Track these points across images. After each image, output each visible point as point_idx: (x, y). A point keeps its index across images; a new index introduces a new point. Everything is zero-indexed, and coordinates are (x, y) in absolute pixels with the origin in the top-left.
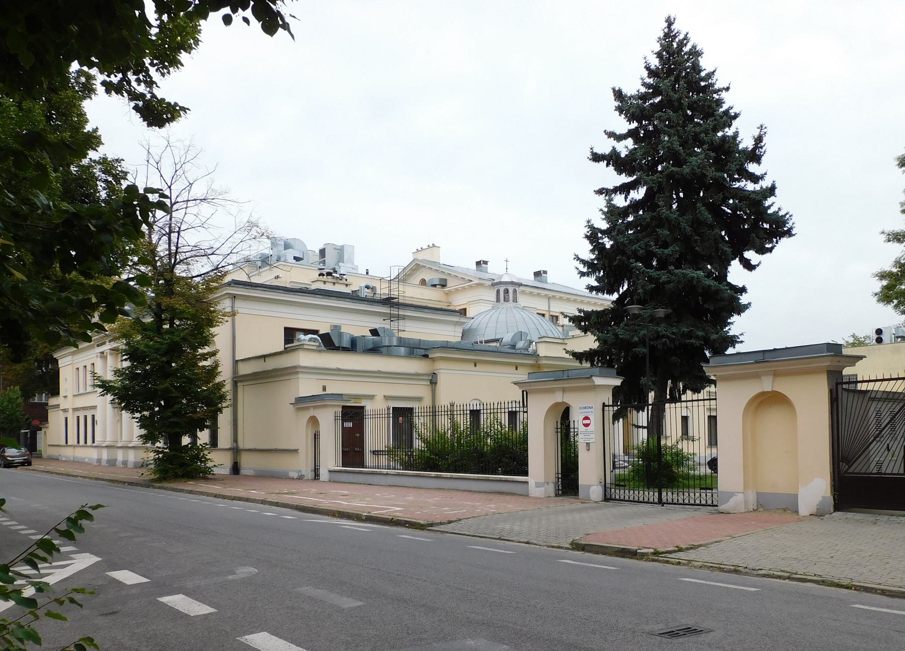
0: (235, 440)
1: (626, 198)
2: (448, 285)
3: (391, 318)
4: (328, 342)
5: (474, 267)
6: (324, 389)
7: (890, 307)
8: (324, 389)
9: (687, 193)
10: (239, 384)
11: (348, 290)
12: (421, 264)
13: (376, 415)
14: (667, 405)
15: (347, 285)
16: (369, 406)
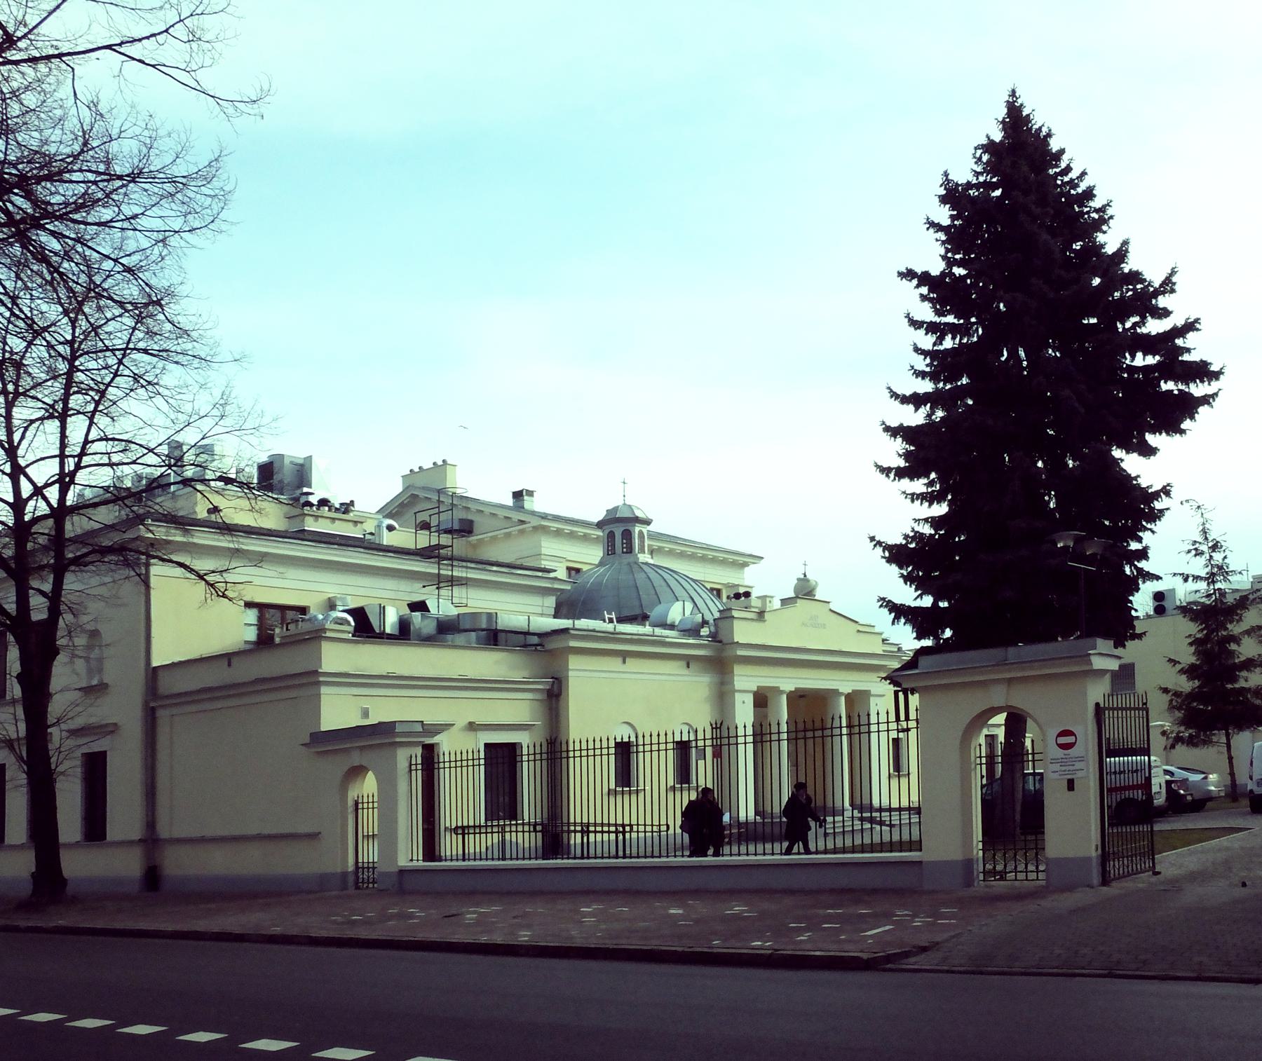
0: (151, 824)
1: (934, 344)
2: (476, 528)
3: (439, 581)
4: (364, 626)
5: (509, 501)
6: (366, 713)
7: (894, 570)
8: (366, 713)
9: (1037, 334)
10: (161, 713)
11: (356, 533)
12: (422, 494)
13: (459, 762)
14: (22, 733)
15: (356, 523)
16: (447, 744)
